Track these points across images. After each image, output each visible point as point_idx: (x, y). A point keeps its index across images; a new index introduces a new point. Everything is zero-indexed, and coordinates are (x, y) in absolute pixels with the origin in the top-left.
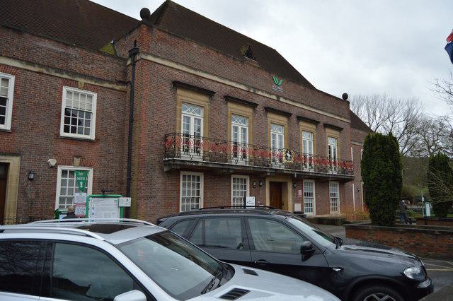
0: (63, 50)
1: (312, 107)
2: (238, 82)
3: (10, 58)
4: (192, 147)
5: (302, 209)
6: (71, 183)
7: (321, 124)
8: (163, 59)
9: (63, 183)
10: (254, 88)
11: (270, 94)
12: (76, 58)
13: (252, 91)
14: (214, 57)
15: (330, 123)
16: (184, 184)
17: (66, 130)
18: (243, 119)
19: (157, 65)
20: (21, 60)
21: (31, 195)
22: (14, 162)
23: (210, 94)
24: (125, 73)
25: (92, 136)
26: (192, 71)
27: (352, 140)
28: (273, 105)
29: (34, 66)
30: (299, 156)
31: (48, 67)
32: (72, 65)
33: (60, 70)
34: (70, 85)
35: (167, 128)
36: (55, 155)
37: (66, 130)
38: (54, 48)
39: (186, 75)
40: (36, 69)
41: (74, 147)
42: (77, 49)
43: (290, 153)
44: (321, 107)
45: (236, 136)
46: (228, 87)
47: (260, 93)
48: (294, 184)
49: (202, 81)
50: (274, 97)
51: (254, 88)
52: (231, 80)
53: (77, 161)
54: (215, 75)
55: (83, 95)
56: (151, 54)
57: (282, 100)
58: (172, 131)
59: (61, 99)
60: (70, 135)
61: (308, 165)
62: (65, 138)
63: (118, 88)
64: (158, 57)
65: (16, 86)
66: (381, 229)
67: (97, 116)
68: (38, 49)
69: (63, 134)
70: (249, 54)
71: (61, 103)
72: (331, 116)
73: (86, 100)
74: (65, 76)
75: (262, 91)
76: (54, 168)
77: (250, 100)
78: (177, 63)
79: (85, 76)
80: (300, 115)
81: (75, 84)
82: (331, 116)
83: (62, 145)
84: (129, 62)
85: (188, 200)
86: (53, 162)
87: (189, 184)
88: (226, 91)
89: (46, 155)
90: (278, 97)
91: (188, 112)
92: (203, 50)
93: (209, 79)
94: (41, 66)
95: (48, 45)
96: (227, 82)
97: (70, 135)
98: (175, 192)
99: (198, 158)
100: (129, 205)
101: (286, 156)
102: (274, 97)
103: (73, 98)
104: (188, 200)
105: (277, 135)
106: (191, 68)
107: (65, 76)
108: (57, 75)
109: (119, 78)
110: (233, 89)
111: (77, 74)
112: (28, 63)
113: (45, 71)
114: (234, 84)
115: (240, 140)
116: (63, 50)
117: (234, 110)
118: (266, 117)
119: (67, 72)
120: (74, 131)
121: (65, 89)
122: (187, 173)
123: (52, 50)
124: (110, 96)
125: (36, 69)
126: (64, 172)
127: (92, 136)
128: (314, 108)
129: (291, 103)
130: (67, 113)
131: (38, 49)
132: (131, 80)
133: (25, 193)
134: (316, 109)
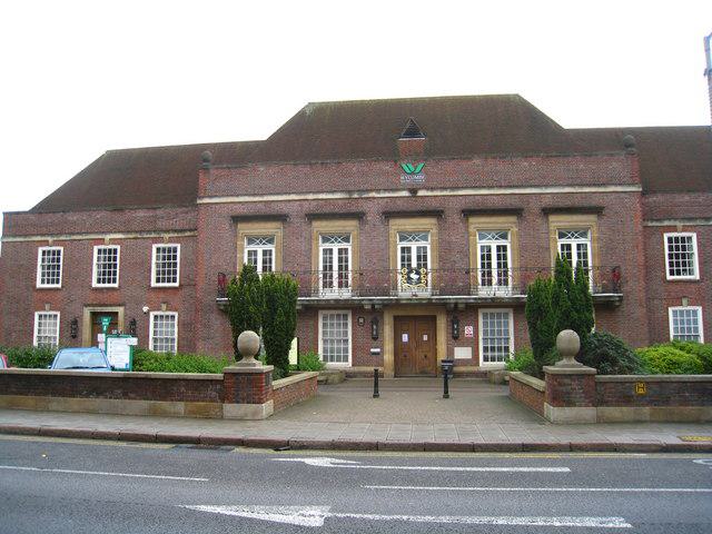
6: (162, 325)
9: (155, 326)
15: (472, 206)
16: (325, 325)
23: (281, 218)
31: (141, 232)
33: (149, 232)
37: (672, 273)
41: (162, 295)
53: (164, 306)
57: (420, 193)
58: (232, 270)
60: (676, 277)
62: (672, 282)
66: (197, 448)
69: (669, 277)
74: (153, 235)
76: (147, 314)
79: (167, 231)
85: (332, 341)
86: (145, 309)
87: (333, 325)
88: (463, 204)
89: (140, 304)
95: (141, 213)
96: (310, 197)
97: (676, 277)
99: (346, 294)
104: (162, 340)
107: (153, 235)
118: (236, 227)
120: (679, 273)
122: (329, 312)
126: (156, 317)
127: (696, 276)
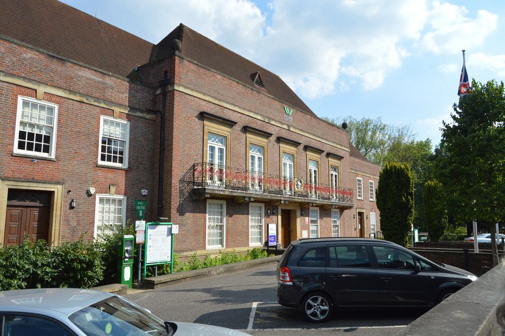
0: (100, 80)
1: (317, 136)
2: (255, 113)
3: (55, 87)
4: (257, 181)
5: (309, 235)
7: (325, 153)
8: (192, 90)
10: (269, 118)
11: (283, 124)
12: (112, 88)
13: (267, 121)
14: (237, 88)
15: (332, 152)
17: (103, 158)
18: (220, 138)
19: (187, 96)
20: (64, 89)
21: (74, 223)
22: (58, 190)
24: (154, 102)
25: (53, 157)
26: (217, 102)
27: (351, 169)
28: (285, 134)
29: (75, 95)
30: (280, 180)
31: (87, 95)
32: (109, 94)
33: (97, 99)
34: (107, 115)
35: (196, 157)
36: (94, 183)
38: (93, 77)
39: (212, 106)
40: (78, 98)
42: (113, 78)
43: (301, 182)
44: (325, 137)
45: (212, 156)
46: (247, 117)
47: (273, 123)
48: (302, 211)
49: (226, 111)
50: (286, 127)
51: (269, 118)
52: (249, 111)
54: (236, 106)
55: (42, 108)
56: (183, 86)
57: (292, 129)
59: (98, 128)
60: (106, 163)
61: (335, 196)
63: (148, 117)
64: (189, 88)
65: (59, 115)
67: (130, 144)
68: (79, 79)
70: (260, 83)
71: (98, 133)
72: (334, 145)
73: (44, 114)
74: (102, 105)
75: (276, 121)
77: (265, 130)
78: (204, 94)
80: (307, 144)
81: (112, 113)
82: (334, 145)
83: (100, 173)
84: (159, 92)
90: (289, 126)
91: (213, 141)
92: (226, 81)
93: (231, 111)
94: (82, 95)
97: (106, 163)
98: (202, 220)
100: (178, 226)
101: (297, 185)
102: (286, 127)
103: (28, 110)
105: (288, 163)
106: (215, 98)
108: (96, 104)
109: (150, 107)
110: (251, 119)
111: (112, 103)
112: (71, 92)
113: (85, 101)
114: (252, 114)
115: (288, 176)
116: (100, 80)
117: (251, 140)
119: (104, 101)
121: (102, 118)
123: (90, 79)
124: (141, 125)
125: (78, 98)
128: (319, 137)
129: (299, 132)
130: (104, 142)
131: (79, 79)
132: (161, 109)
133: (68, 221)
134: (321, 138)
